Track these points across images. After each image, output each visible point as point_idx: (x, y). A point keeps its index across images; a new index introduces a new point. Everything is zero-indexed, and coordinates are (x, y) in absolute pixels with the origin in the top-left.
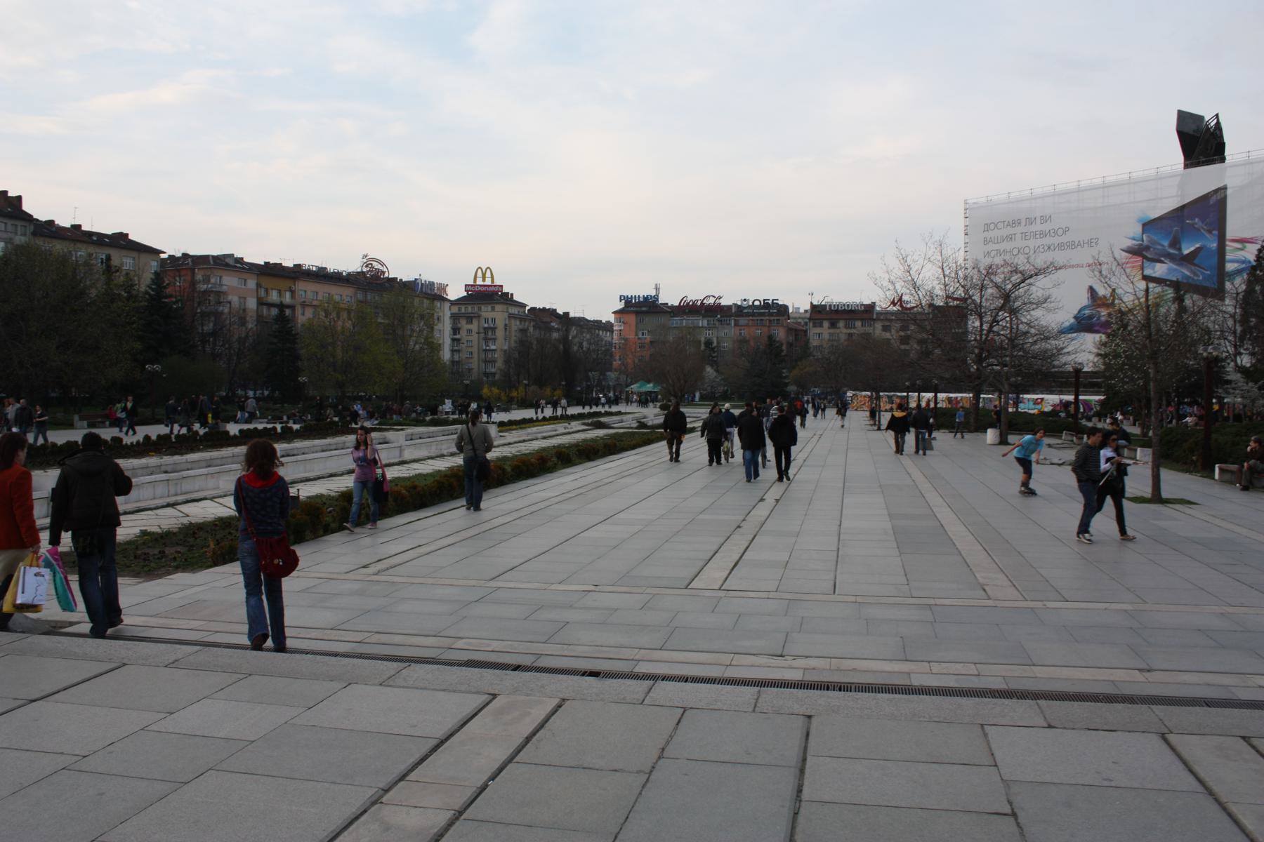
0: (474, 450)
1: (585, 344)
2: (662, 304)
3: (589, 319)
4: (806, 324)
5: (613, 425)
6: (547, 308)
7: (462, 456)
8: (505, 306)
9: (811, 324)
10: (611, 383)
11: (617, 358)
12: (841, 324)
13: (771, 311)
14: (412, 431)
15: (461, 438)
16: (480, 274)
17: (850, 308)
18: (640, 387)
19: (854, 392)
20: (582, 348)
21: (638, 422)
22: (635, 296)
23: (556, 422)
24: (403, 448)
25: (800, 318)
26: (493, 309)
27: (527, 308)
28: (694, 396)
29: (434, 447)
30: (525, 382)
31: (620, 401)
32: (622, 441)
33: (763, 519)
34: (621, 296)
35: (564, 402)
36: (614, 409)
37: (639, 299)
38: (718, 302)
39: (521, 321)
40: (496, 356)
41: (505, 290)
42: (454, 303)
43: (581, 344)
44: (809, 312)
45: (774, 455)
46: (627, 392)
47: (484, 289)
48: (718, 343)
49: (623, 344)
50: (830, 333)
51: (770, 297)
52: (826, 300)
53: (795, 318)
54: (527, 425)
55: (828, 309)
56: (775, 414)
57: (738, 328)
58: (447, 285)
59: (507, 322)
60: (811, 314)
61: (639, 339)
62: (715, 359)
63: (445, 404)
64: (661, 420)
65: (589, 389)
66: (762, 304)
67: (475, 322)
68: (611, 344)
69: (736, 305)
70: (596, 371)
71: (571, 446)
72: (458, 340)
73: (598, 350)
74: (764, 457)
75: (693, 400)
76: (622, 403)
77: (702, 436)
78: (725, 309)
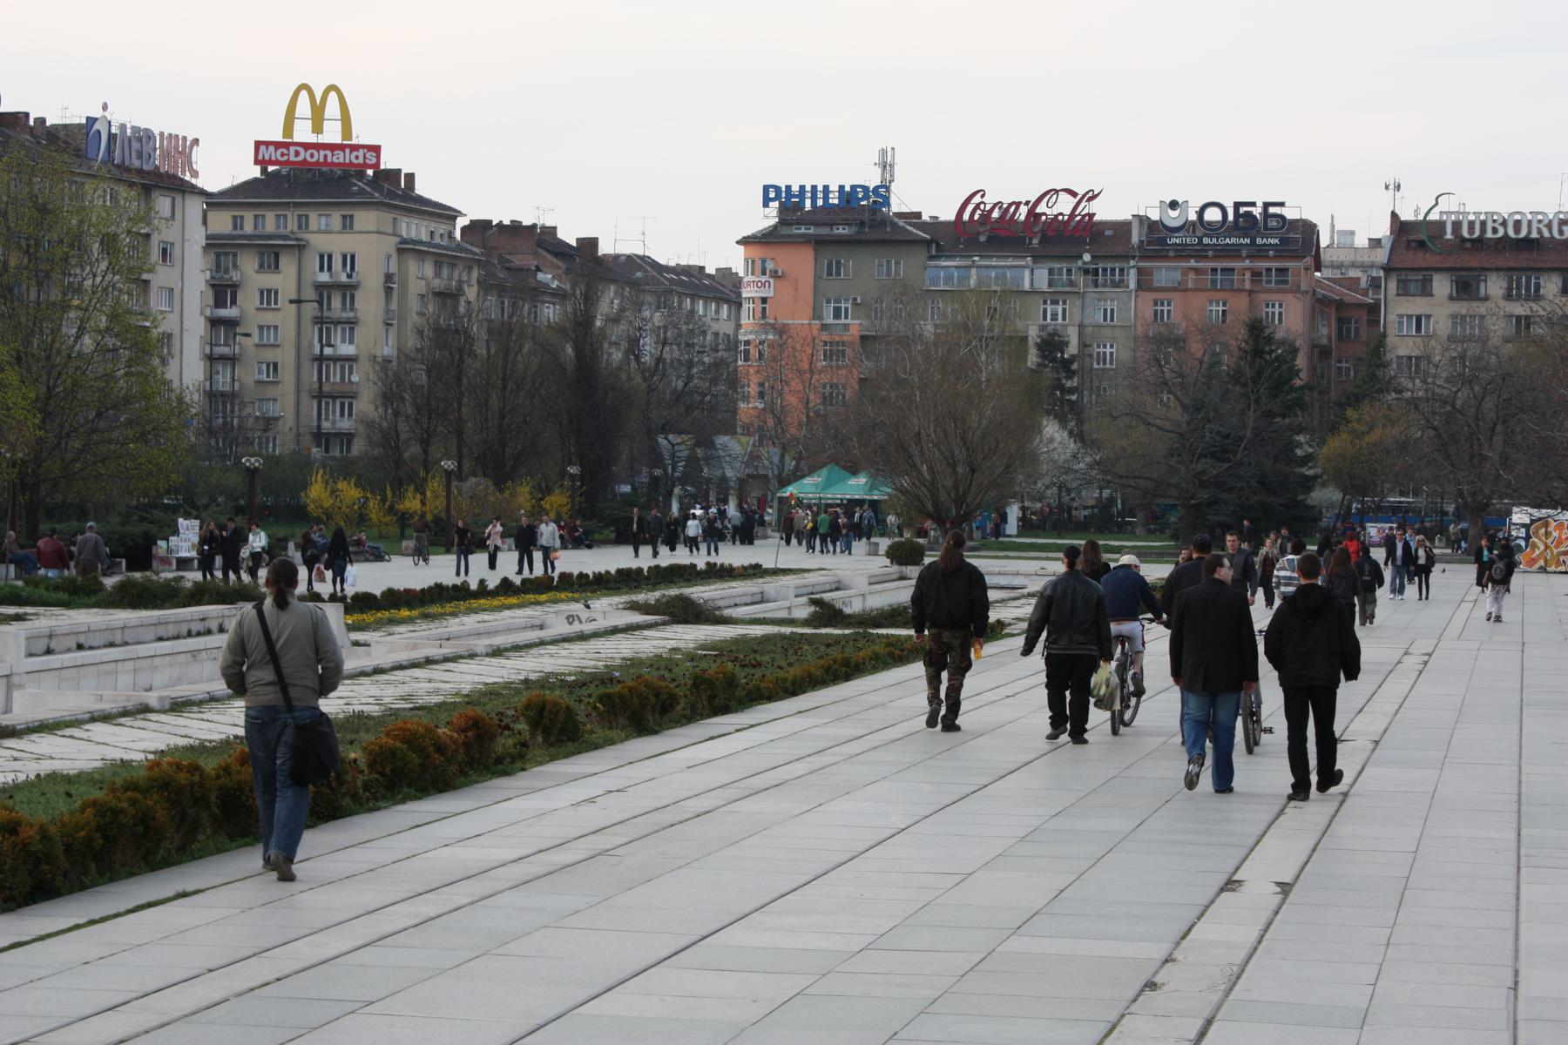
0: (282, 683)
1: (648, 345)
2: (900, 215)
3: (662, 260)
4: (1375, 284)
5: (727, 612)
6: (527, 222)
7: (240, 704)
8: (387, 216)
9: (1392, 285)
10: (729, 473)
11: (753, 389)
12: (1494, 286)
13: (1259, 241)
14: (52, 623)
15: (240, 649)
16: (304, 107)
17: (1523, 234)
18: (828, 484)
19: (1536, 513)
20: (637, 358)
21: (814, 602)
22: (814, 188)
23: (544, 597)
24: (16, 679)
25: (1353, 265)
26: (348, 223)
27: (461, 222)
28: (1003, 518)
29: (125, 680)
30: (448, 464)
31: (758, 530)
32: (758, 665)
33: (1239, 958)
34: (766, 188)
35: (548, 532)
36: (732, 555)
37: (826, 198)
38: (1085, 209)
39: (438, 265)
40: (355, 378)
41: (387, 162)
42: (216, 201)
43: (633, 346)
44: (1387, 245)
45: (1283, 708)
46: (781, 500)
47: (319, 156)
48: (1083, 345)
49: (771, 345)
50: (1454, 316)
51: (1258, 195)
53: (1340, 266)
54: (449, 608)
55: (1449, 236)
56: (1289, 581)
57: (1149, 297)
58: (196, 142)
59: (393, 269)
60: (1392, 249)
61: (824, 327)
62: (1074, 398)
63: (176, 532)
64: (902, 594)
65: (659, 490)
66: (1231, 217)
67: (288, 264)
68: (732, 344)
69: (1142, 220)
70: (680, 433)
71: (585, 681)
72: (231, 324)
73: (690, 364)
74: (1253, 716)
75: (998, 531)
76: (765, 537)
77: (1028, 650)
78: (1108, 233)
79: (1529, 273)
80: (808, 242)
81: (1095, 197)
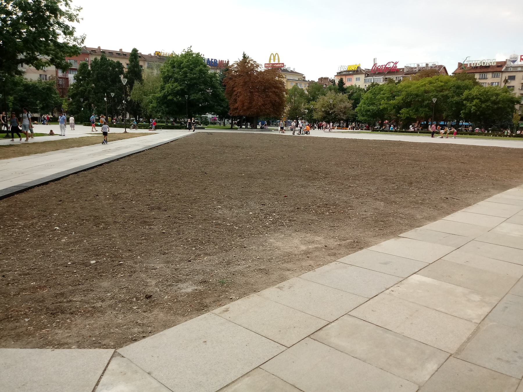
16: (272, 57)
52: (468, 59)
79: (485, 73)
80: (344, 75)
81: (397, 63)
